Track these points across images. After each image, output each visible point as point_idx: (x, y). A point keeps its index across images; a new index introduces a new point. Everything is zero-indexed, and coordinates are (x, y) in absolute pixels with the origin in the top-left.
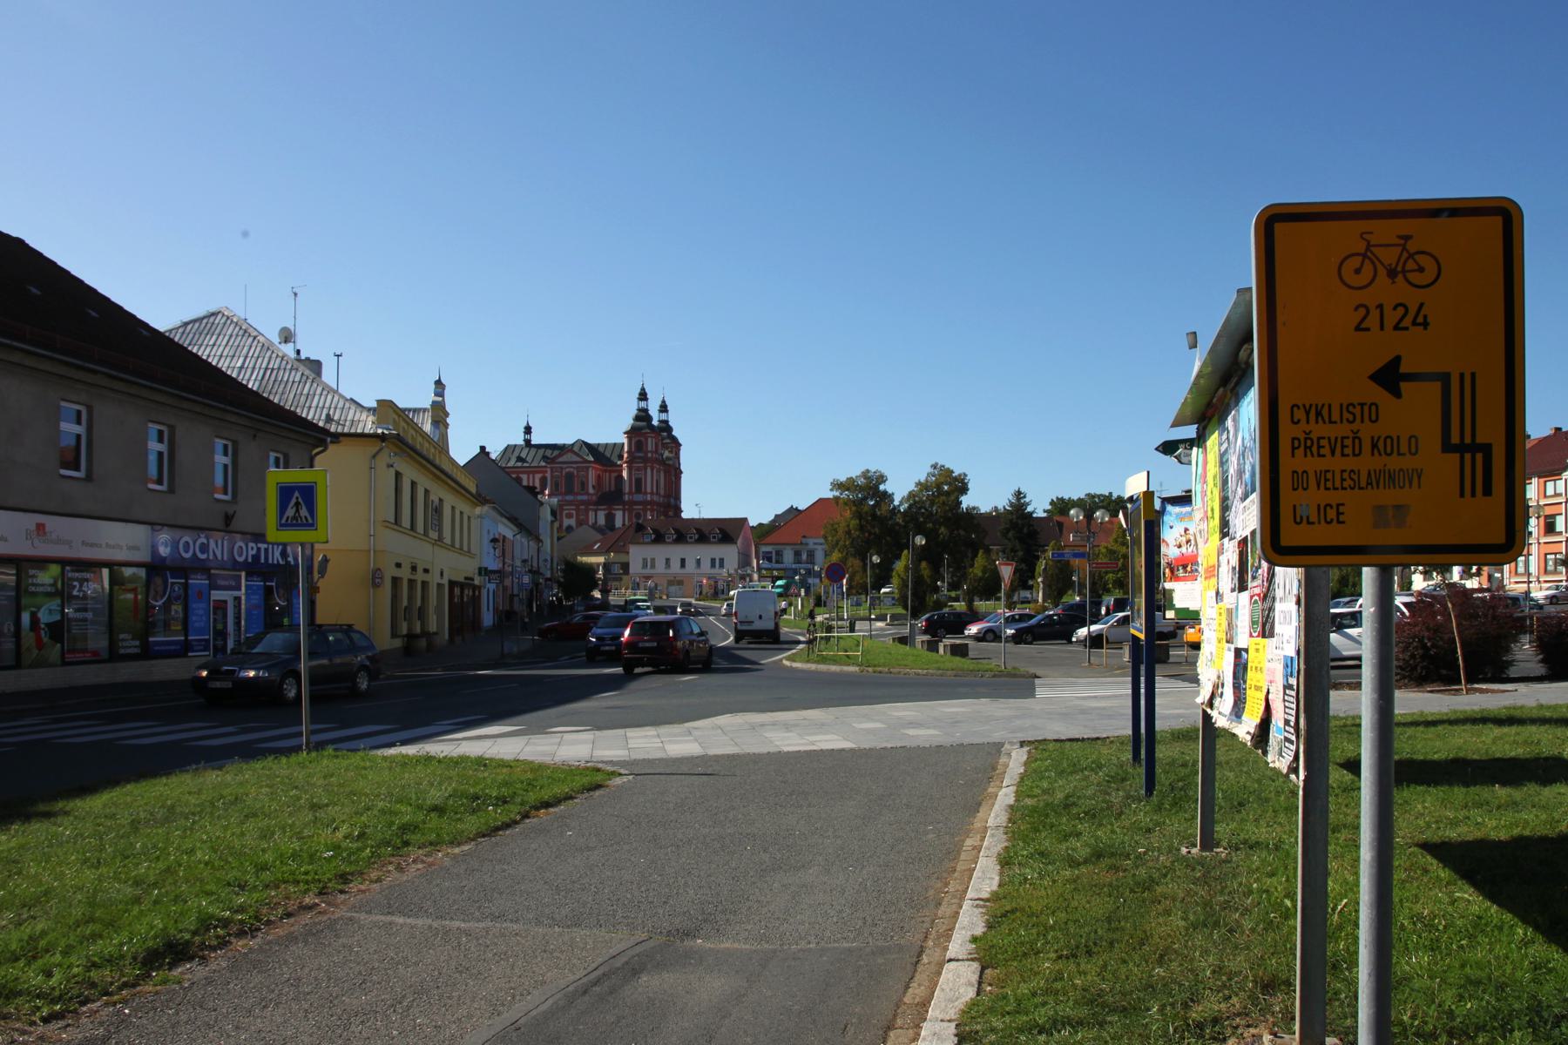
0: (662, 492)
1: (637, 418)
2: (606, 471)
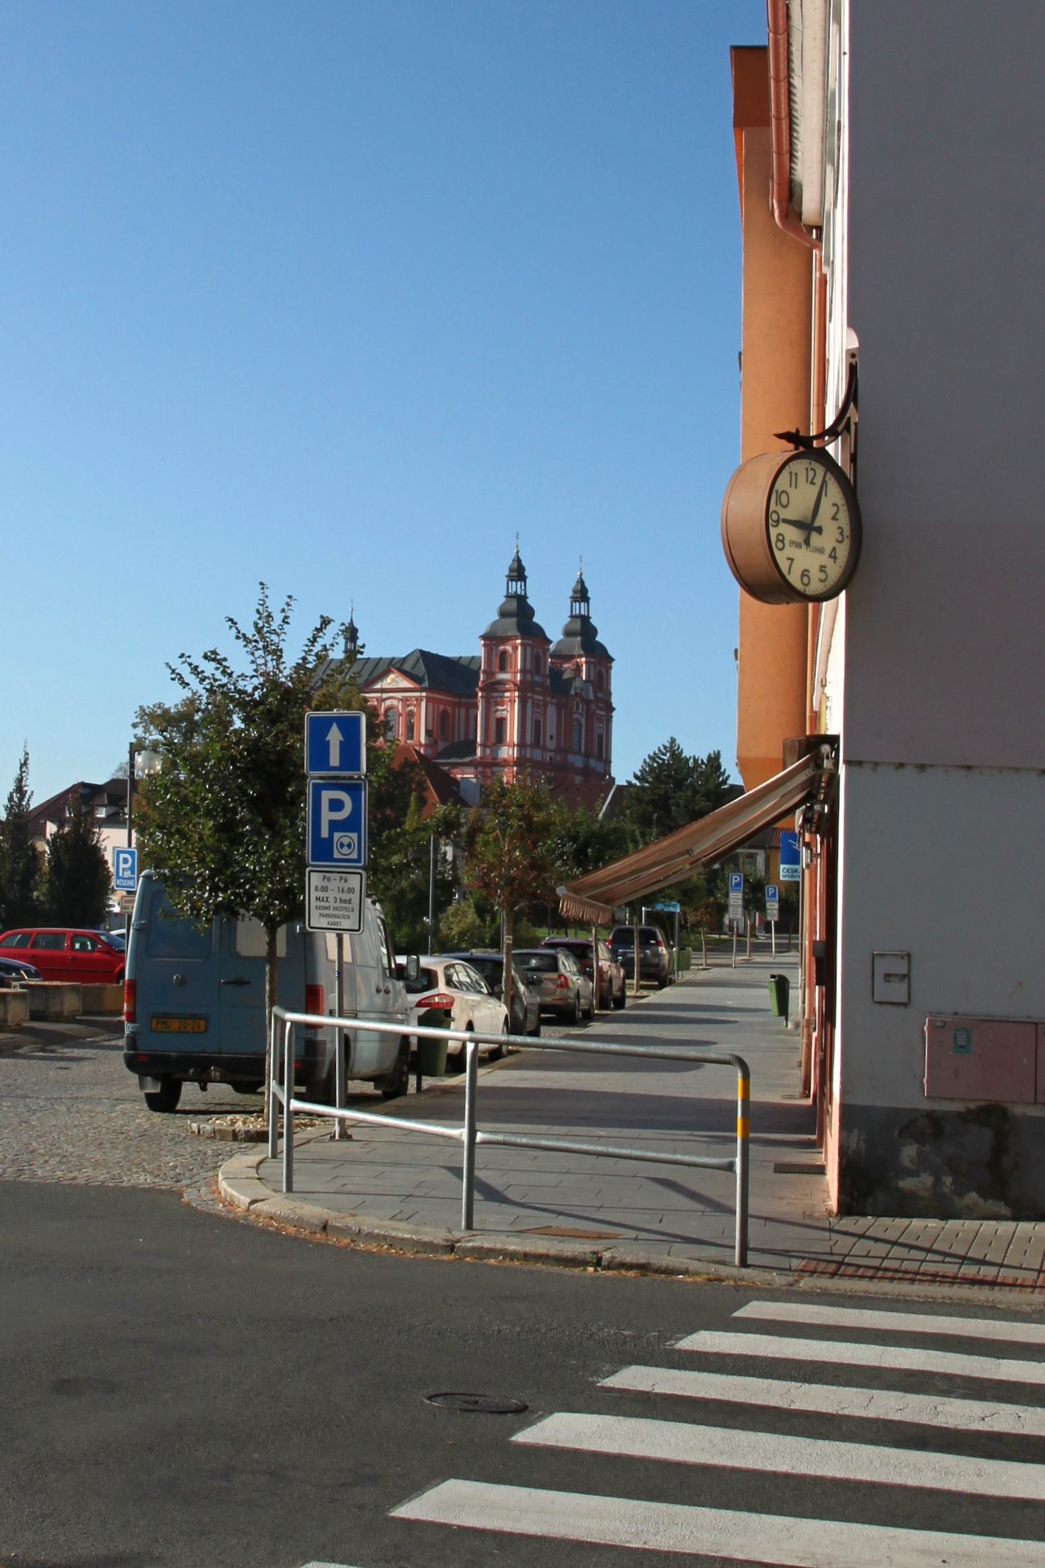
0: (551, 744)
1: (503, 614)
2: (459, 705)
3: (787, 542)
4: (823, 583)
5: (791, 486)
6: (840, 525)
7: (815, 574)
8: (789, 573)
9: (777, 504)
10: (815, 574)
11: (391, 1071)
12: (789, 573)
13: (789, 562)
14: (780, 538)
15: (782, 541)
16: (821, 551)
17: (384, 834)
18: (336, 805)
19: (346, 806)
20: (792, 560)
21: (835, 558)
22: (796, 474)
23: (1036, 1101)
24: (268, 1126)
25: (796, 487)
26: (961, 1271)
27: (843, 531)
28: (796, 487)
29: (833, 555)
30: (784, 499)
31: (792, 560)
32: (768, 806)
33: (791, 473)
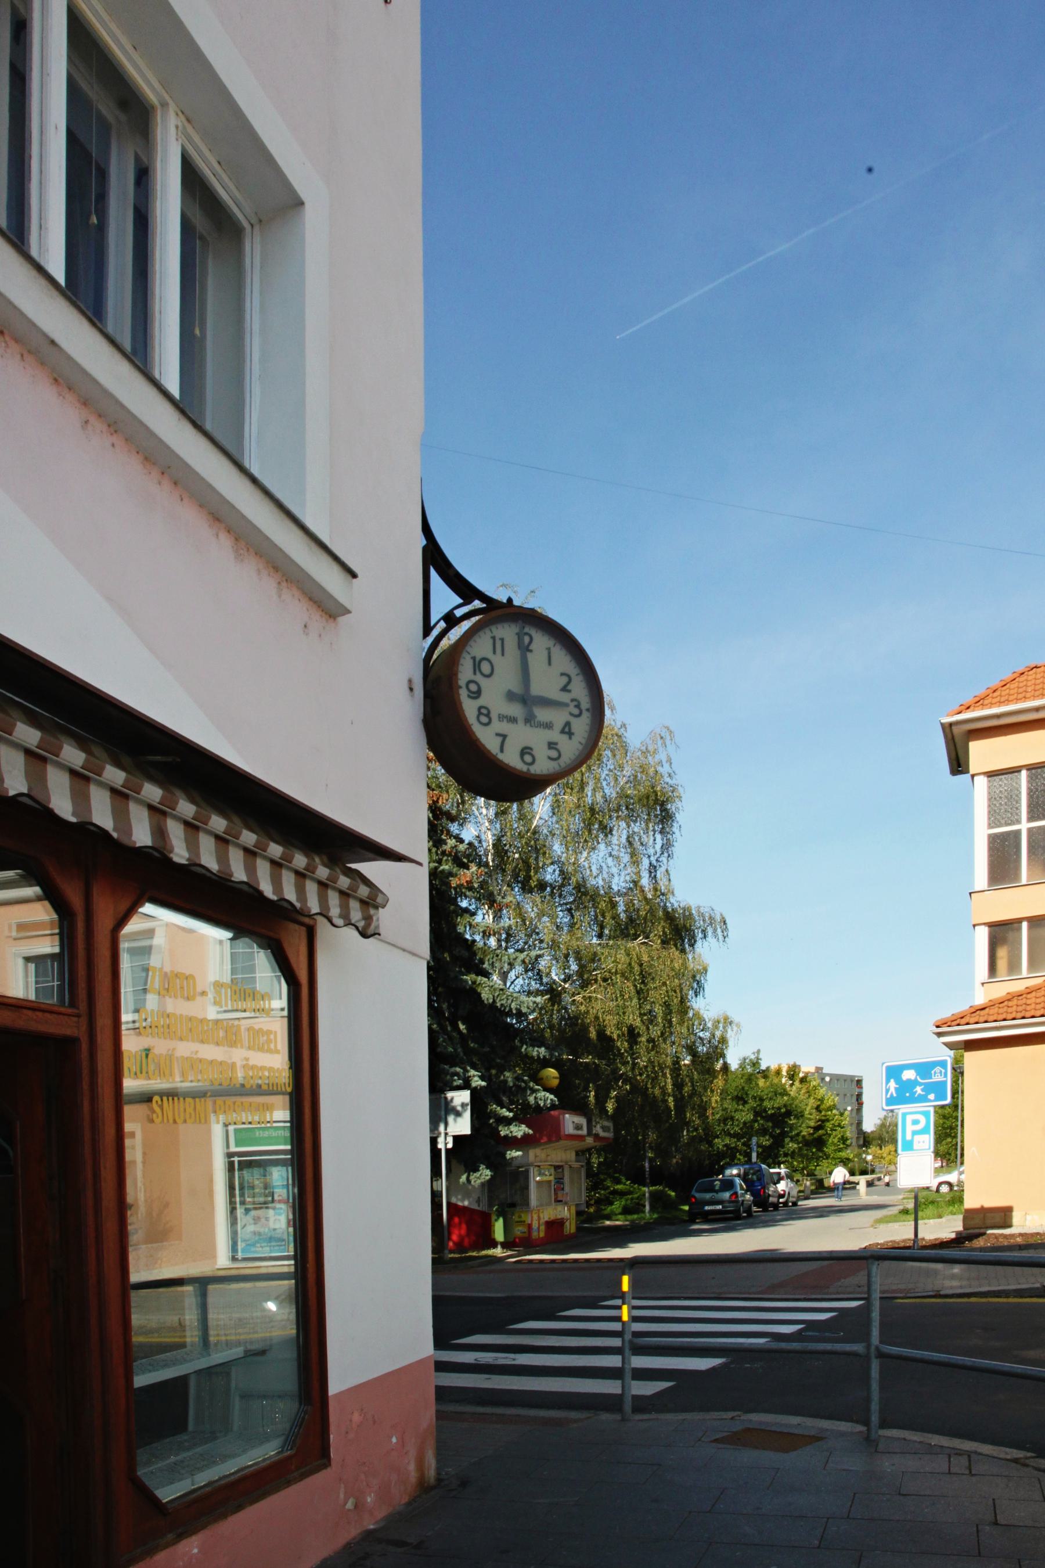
3: (494, 716)
4: (556, 762)
5: (494, 652)
6: (562, 671)
7: (542, 753)
8: (502, 750)
9: (475, 673)
10: (542, 753)
11: (493, 1237)
12: (502, 750)
13: (500, 739)
14: (484, 711)
15: (488, 715)
16: (549, 726)
17: (820, 1132)
18: (916, 1122)
19: (921, 1120)
20: (504, 737)
21: (570, 734)
22: (502, 640)
23: (969, 1456)
24: (946, 1075)
25: (503, 655)
26: (278, 1184)
27: (579, 702)
28: (503, 655)
29: (567, 730)
30: (486, 668)
31: (504, 737)
32: (38, 709)
33: (494, 638)
